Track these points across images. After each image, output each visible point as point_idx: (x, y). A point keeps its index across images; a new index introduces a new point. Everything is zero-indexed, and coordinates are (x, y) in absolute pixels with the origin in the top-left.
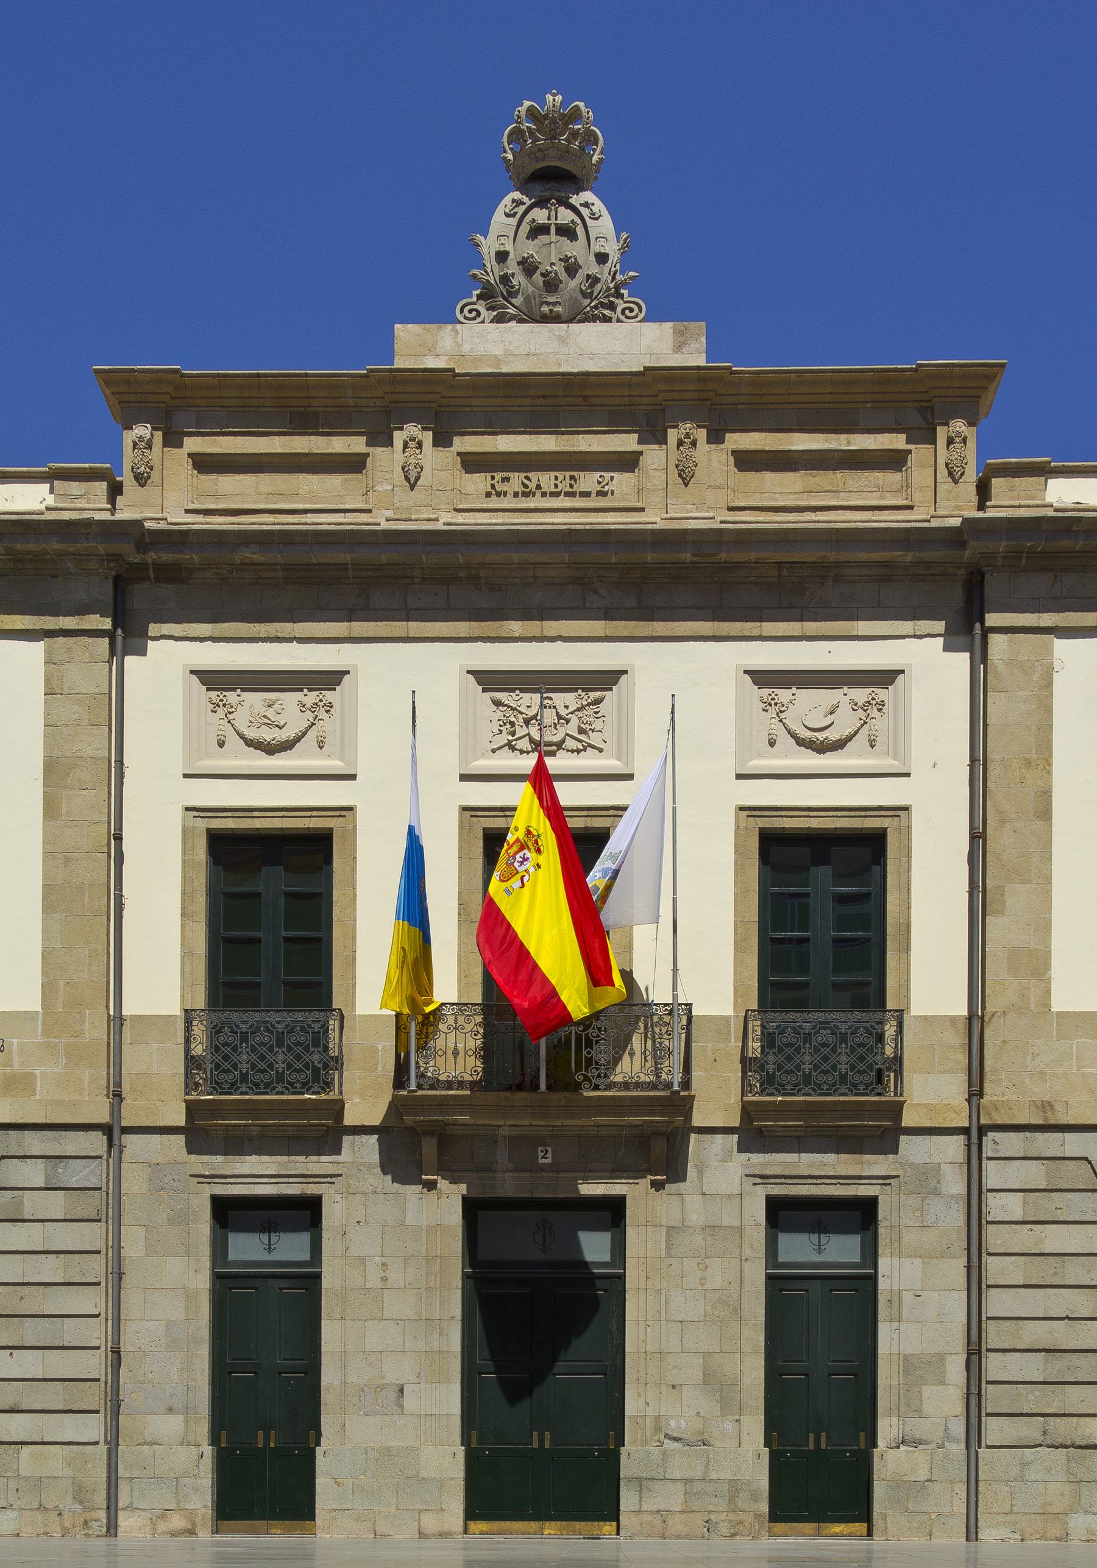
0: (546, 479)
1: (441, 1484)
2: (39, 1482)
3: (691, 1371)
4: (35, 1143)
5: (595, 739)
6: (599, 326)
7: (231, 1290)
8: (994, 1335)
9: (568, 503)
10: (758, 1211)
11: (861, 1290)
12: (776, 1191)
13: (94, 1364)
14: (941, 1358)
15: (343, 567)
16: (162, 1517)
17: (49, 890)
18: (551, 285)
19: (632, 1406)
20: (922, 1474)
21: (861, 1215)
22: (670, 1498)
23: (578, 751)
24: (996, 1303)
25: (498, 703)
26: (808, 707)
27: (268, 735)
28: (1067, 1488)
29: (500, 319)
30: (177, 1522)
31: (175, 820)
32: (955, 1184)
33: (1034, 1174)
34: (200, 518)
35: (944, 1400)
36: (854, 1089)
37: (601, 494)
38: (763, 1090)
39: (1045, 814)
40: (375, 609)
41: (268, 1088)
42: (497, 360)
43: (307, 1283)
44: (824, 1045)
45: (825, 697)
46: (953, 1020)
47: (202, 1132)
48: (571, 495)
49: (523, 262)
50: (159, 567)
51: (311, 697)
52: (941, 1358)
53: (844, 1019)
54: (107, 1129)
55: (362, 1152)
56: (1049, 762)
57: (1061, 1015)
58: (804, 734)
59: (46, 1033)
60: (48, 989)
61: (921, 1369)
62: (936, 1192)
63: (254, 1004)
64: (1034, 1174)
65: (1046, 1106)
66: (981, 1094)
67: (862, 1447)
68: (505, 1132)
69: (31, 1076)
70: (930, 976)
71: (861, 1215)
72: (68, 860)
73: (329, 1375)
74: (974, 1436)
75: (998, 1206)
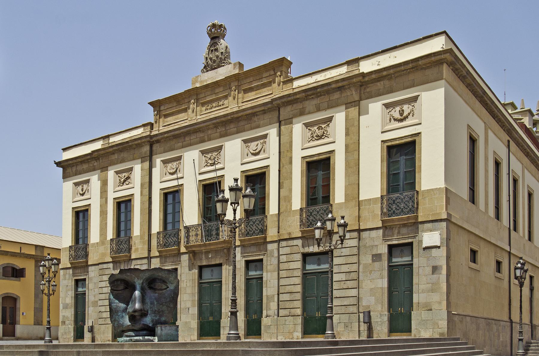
1: (194, 329)
6: (222, 68)
11: (326, 276)
12: (246, 259)
14: (274, 295)
15: (180, 134)
18: (214, 62)
20: (270, 324)
26: (253, 146)
27: (172, 171)
28: (293, 326)
29: (207, 71)
32: (276, 254)
33: (287, 250)
35: (274, 306)
38: (309, 226)
41: (400, 214)
42: (206, 81)
43: (260, 279)
45: (255, 143)
46: (376, 199)
47: (386, 227)
48: (218, 106)
50: (156, 141)
52: (274, 295)
53: (409, 193)
55: (185, 259)
56: (291, 150)
57: (293, 211)
58: (252, 152)
62: (273, 256)
64: (287, 250)
65: (290, 234)
66: (150, 251)
68: (203, 251)
70: (339, 195)
75: (283, 258)
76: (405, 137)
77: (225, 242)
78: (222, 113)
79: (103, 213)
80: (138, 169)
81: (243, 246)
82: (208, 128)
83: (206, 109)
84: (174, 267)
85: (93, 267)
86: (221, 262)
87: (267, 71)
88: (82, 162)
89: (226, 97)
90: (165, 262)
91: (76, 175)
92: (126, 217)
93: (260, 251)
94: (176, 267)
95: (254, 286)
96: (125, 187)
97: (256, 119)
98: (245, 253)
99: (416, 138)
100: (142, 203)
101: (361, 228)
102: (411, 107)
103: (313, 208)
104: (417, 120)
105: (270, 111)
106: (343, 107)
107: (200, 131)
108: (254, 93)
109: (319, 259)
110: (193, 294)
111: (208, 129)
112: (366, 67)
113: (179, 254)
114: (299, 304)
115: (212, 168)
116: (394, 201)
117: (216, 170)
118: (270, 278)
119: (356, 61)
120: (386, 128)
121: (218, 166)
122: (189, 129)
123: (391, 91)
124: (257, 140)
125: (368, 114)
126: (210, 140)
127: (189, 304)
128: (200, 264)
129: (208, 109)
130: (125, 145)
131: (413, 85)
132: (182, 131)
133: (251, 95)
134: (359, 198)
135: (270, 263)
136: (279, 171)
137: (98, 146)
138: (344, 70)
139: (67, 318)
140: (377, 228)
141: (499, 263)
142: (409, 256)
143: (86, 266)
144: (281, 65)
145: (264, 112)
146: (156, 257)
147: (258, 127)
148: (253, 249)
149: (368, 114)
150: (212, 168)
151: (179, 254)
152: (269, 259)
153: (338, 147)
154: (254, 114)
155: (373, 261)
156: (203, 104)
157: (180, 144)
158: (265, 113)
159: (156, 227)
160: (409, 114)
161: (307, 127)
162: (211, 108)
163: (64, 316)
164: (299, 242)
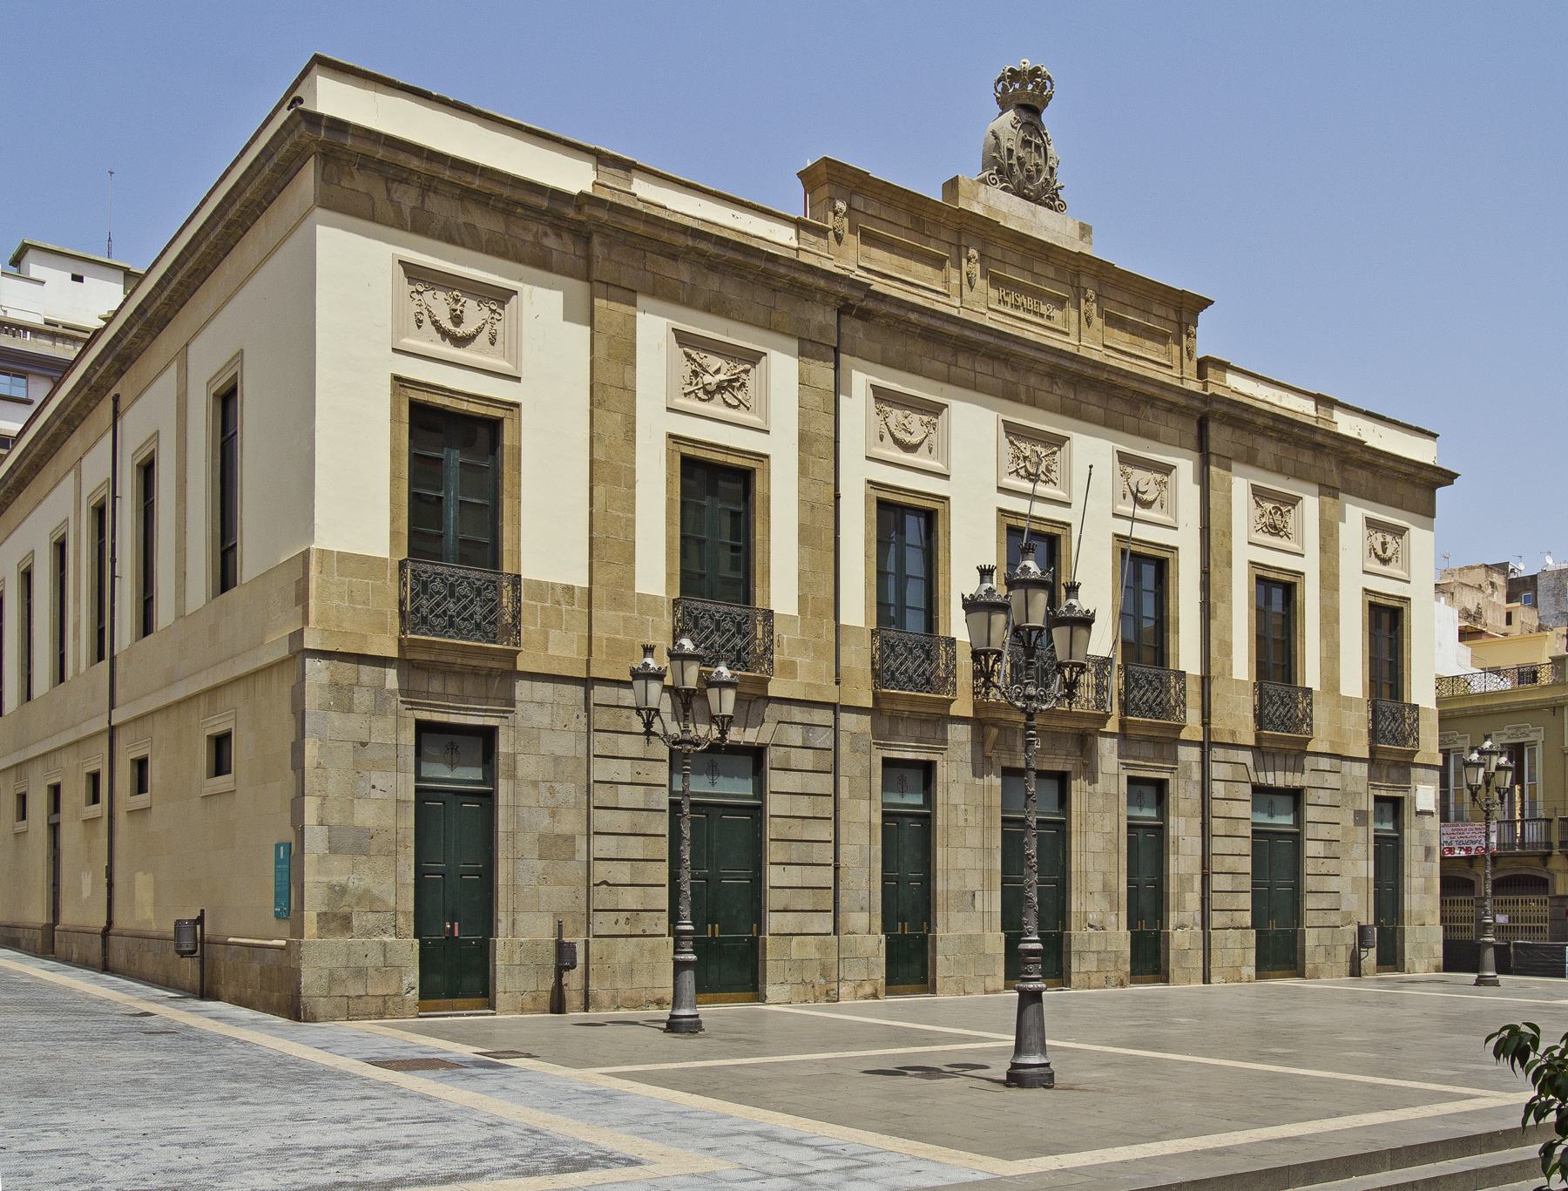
0: (1028, 302)
1: (994, 958)
3: (1096, 885)
4: (798, 714)
5: (1053, 476)
7: (1262, 837)
8: (1216, 864)
9: (1007, 310)
10: (409, 737)
12: (1131, 773)
13: (825, 876)
14: (1192, 875)
16: (860, 986)
17: (802, 528)
19: (1075, 905)
20: (1187, 946)
21: (1296, 796)
22: (1090, 964)
23: (735, 407)
24: (1217, 845)
25: (688, 356)
30: (868, 989)
31: (1108, 543)
34: (864, 274)
35: (1193, 900)
36: (460, 634)
37: (1049, 317)
39: (1230, 565)
40: (389, 191)
44: (438, 593)
49: (1019, 158)
52: (1192, 875)
54: (1201, 744)
55: (960, 735)
59: (803, 632)
60: (802, 600)
61: (1184, 881)
63: (438, 557)
67: (1545, 911)
69: (793, 663)
71: (1296, 796)
72: (813, 507)
73: (940, 886)
74: (1205, 922)
76: (727, 448)
77: (1081, 716)
78: (1031, 333)
79: (609, 471)
80: (782, 370)
81: (1123, 735)
82: (1030, 366)
83: (1001, 301)
84: (923, 757)
85: (545, 690)
86: (1068, 768)
87: (1162, 303)
88: (467, 195)
89: (1060, 303)
90: (893, 734)
91: (707, 309)
92: (1138, 605)
93: (1164, 760)
94: (932, 757)
95: (1147, 848)
96: (715, 408)
97: (1149, 412)
98: (1127, 757)
99: (1297, 580)
100: (1227, 598)
101: (595, 673)
102: (486, 313)
103: (462, 573)
104: (506, 364)
105: (1181, 414)
106: (794, 345)
107: (1006, 361)
108: (1126, 337)
109: (1271, 803)
110: (986, 851)
111: (1030, 370)
112: (1346, 425)
113: (941, 719)
114: (1246, 901)
115: (1026, 486)
116: (718, 622)
117: (1033, 497)
118: (1183, 829)
119: (629, 167)
120: (406, 340)
121: (1041, 489)
122: (991, 339)
123: (716, 307)
124: (1148, 470)
125: (565, 319)
126: (1032, 403)
127: (973, 882)
128: (1007, 764)
129: (1005, 303)
130: (756, 262)
131: (770, 327)
132: (967, 333)
133: (1121, 339)
134: (837, 617)
135: (1183, 796)
136: (837, 497)
137: (1303, 408)
138: (784, 235)
139: (369, 900)
140: (1361, 760)
141: (141, 786)
142: (916, 792)
143: (501, 676)
144: (1184, 309)
145: (1172, 408)
146: (1112, 735)
147: (1153, 436)
148: (1146, 749)
149: (565, 319)
150: (1026, 486)
151: (941, 719)
152: (1181, 783)
153: (1310, 566)
154: (1150, 400)
155: (1357, 823)
156: (996, 281)
157: (939, 366)
158: (1170, 411)
159: (856, 609)
160: (479, 330)
161: (1008, 433)
162: (1017, 307)
163: (339, 891)
164: (1246, 757)
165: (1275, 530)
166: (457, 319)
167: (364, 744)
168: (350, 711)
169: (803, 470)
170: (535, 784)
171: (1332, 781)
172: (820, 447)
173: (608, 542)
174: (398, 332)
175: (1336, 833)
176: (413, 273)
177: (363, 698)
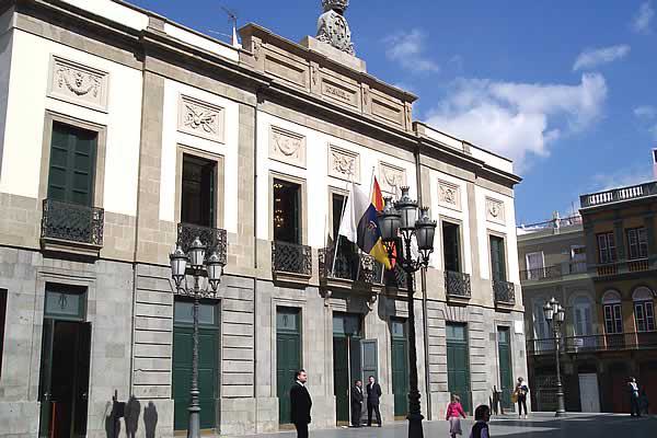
2: (238, 412)
11: (212, 337)
26: (71, 75)
51: (296, 141)
79: (148, 159)
112: (476, 154)
121: (453, 206)
137: (458, 146)
165: (449, 200)
166: (79, 84)
167: (18, 295)
168: (11, 277)
169: (240, 164)
170: (105, 317)
171: (480, 318)
172: (249, 152)
173: (146, 194)
174: (51, 87)
175: (482, 344)
176: (59, 60)
177: (19, 271)
